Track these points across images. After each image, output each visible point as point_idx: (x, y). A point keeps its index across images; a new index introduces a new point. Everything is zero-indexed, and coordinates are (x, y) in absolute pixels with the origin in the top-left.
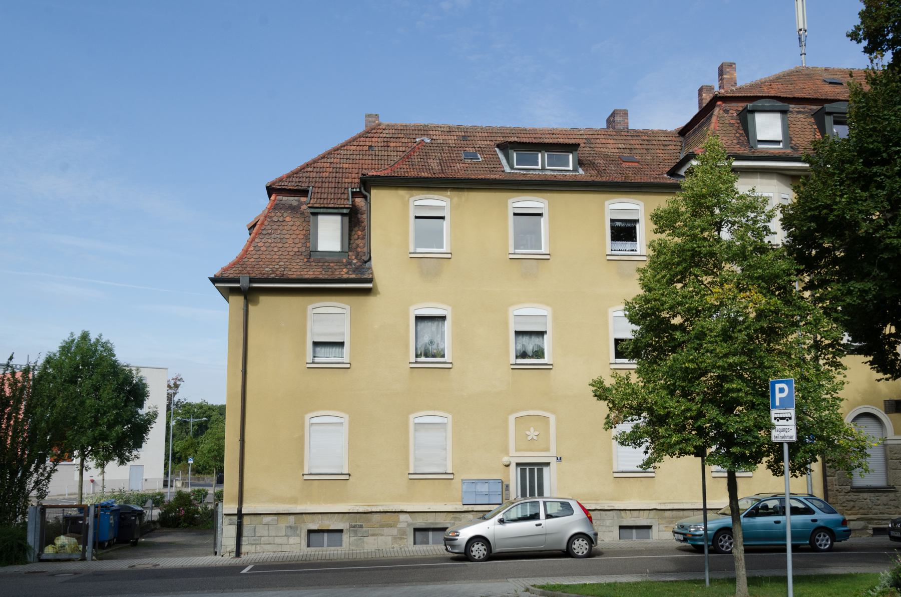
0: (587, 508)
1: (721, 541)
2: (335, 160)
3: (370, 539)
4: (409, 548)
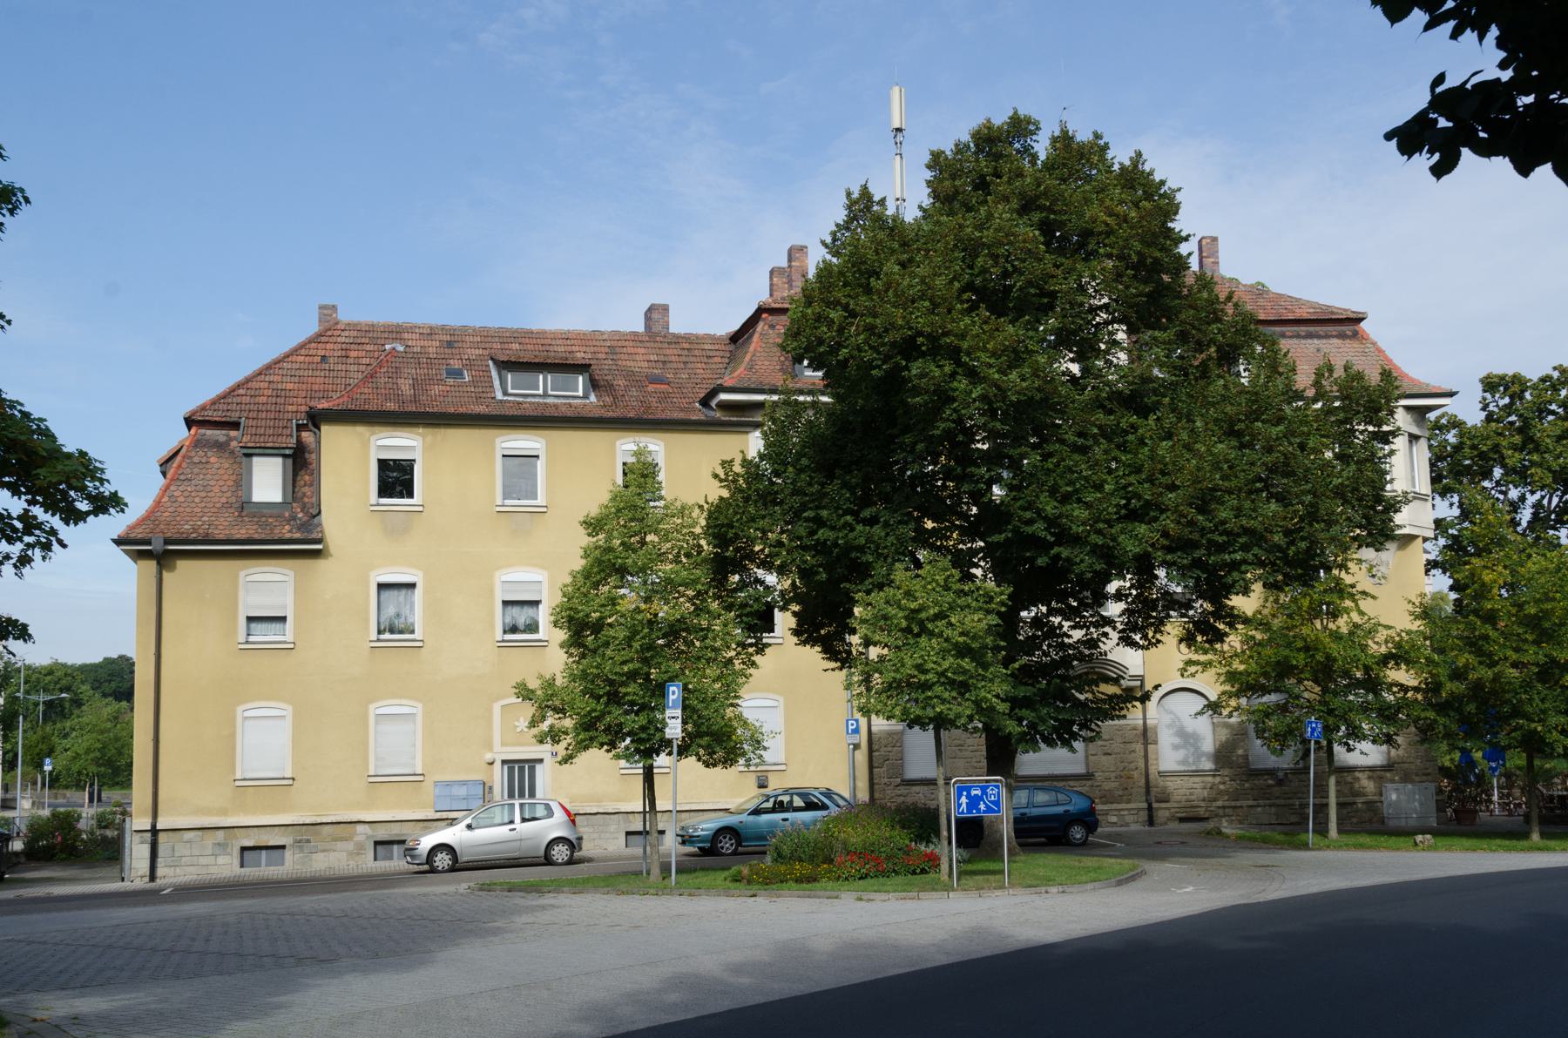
2: (276, 378)
3: (320, 856)
4: (368, 863)
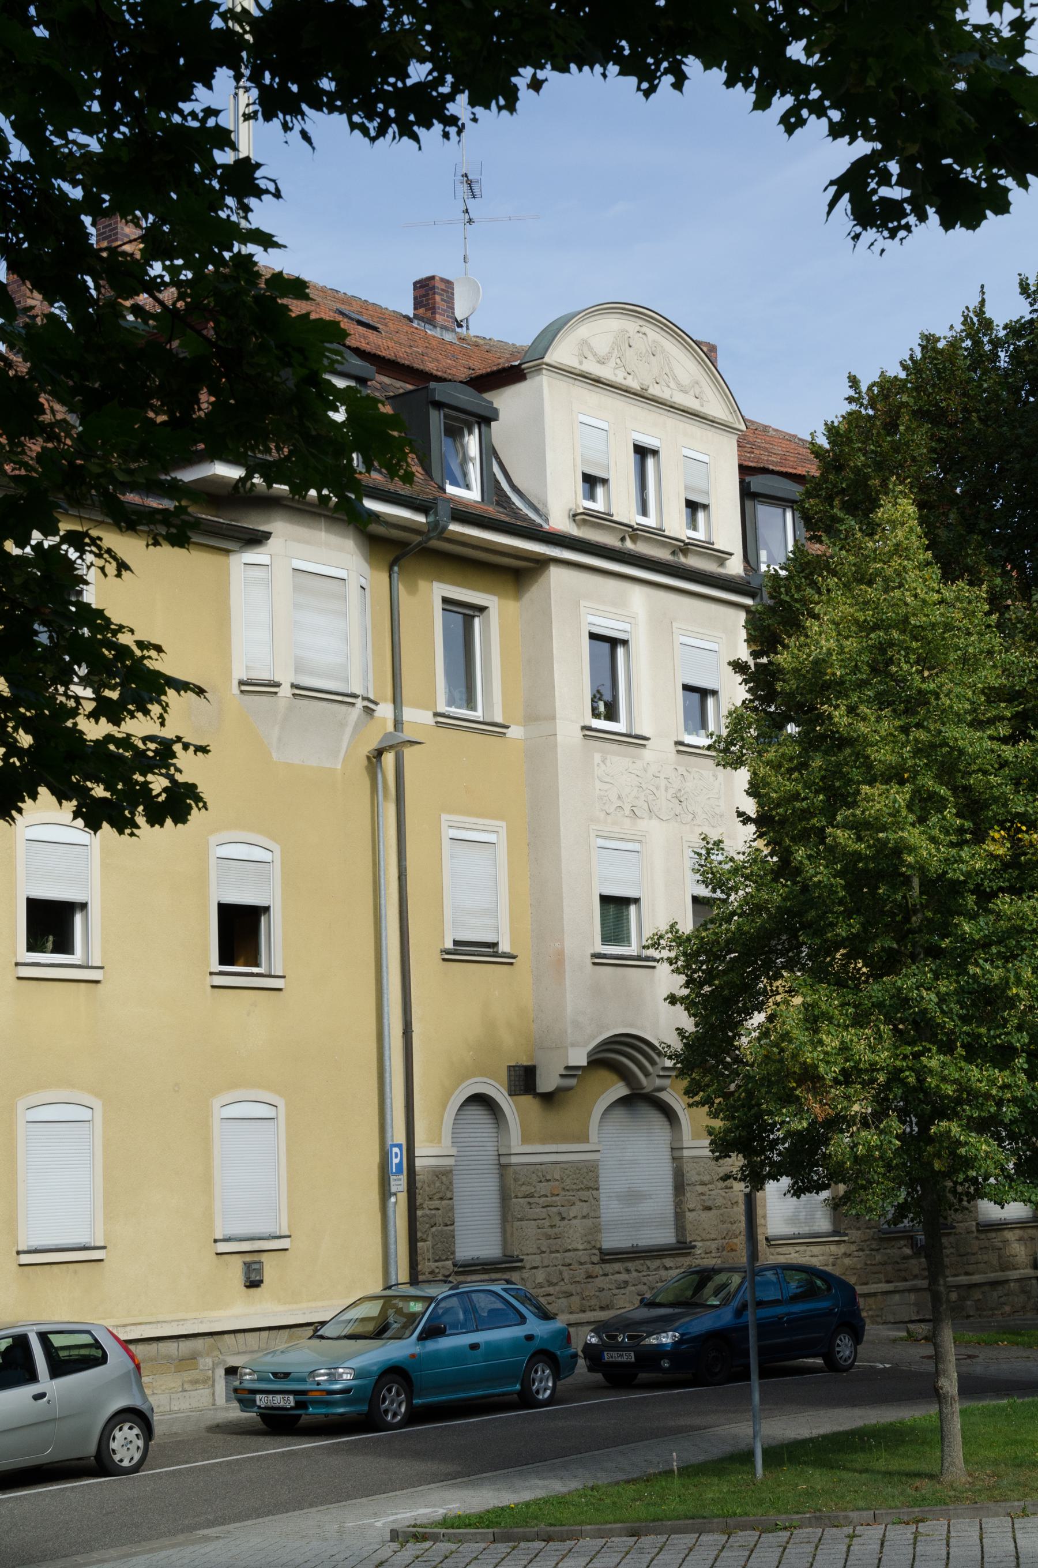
0: (123, 1337)
1: (384, 1400)
